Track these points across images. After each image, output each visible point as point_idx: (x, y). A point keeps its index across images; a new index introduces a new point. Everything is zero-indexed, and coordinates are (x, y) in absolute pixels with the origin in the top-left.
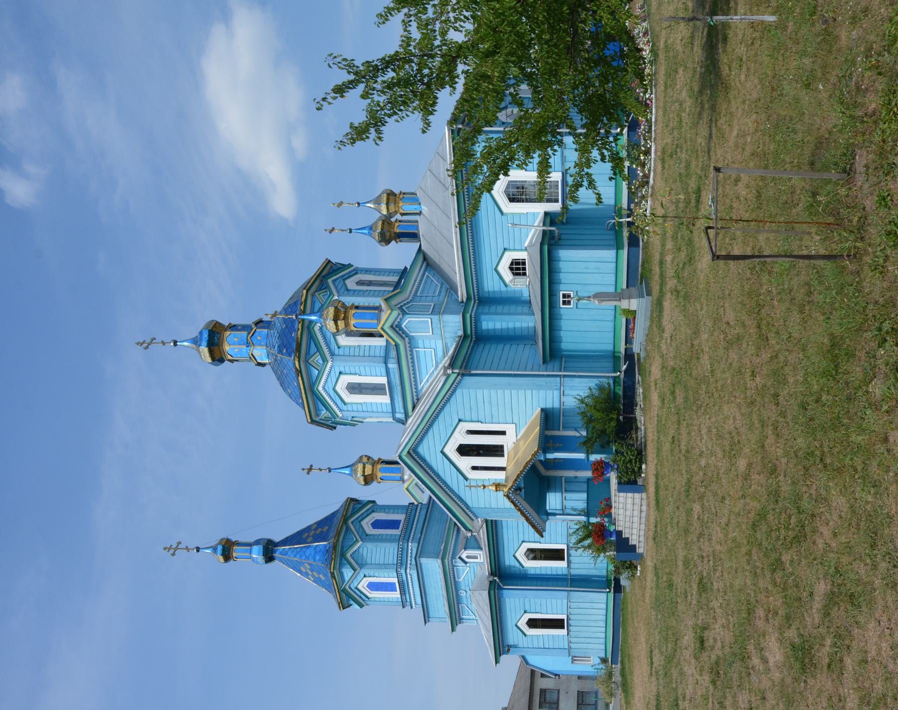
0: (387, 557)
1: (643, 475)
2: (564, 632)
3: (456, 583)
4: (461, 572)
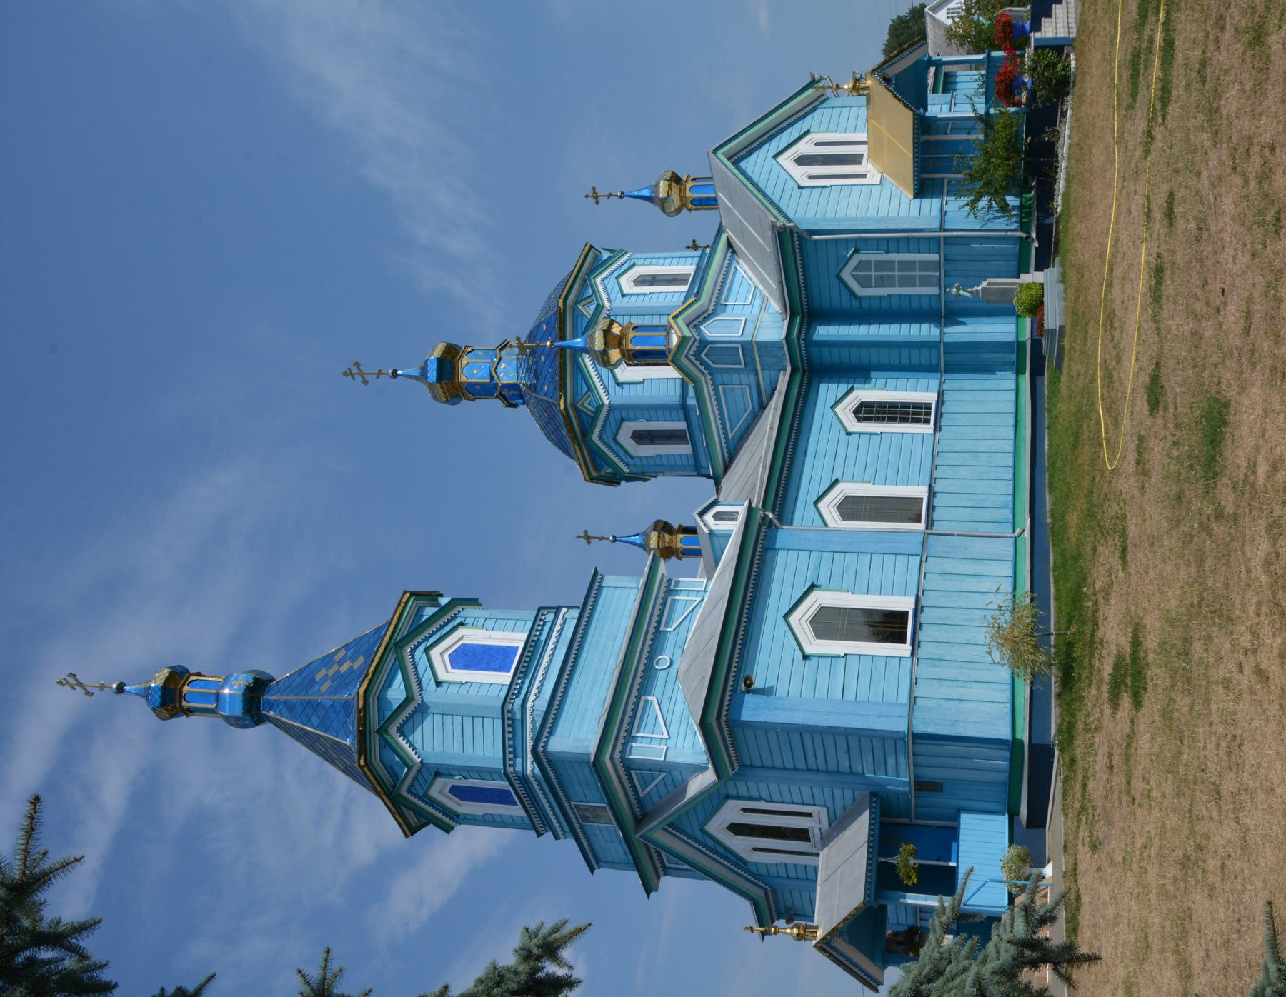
4: (679, 607)
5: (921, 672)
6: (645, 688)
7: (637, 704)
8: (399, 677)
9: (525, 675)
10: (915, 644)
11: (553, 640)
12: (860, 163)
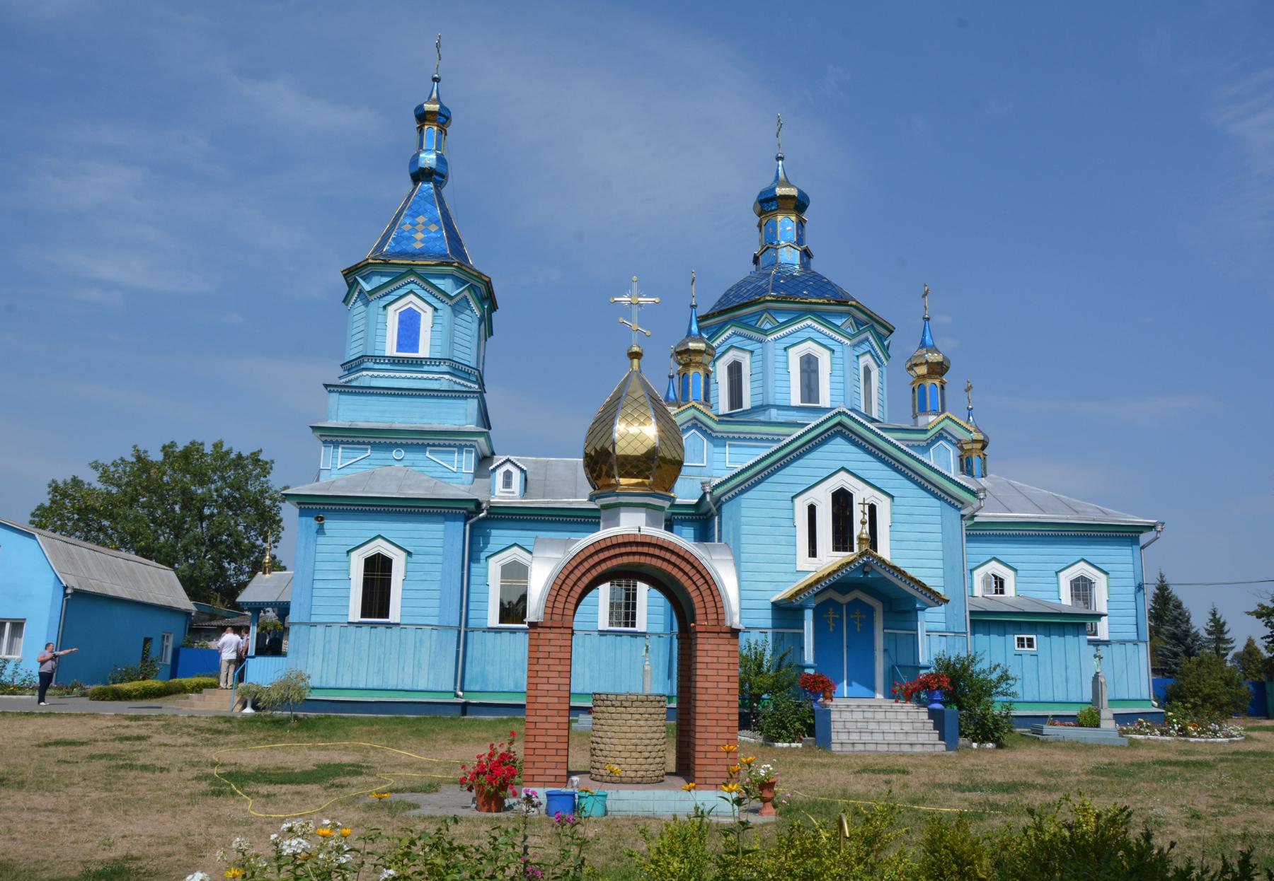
0: (461, 348)
1: (975, 745)
2: (355, 613)
3: (422, 448)
4: (448, 457)
5: (336, 628)
6: (375, 446)
7: (364, 443)
8: (385, 280)
9: (393, 363)
10: (359, 625)
11: (425, 376)
12: (837, 547)
